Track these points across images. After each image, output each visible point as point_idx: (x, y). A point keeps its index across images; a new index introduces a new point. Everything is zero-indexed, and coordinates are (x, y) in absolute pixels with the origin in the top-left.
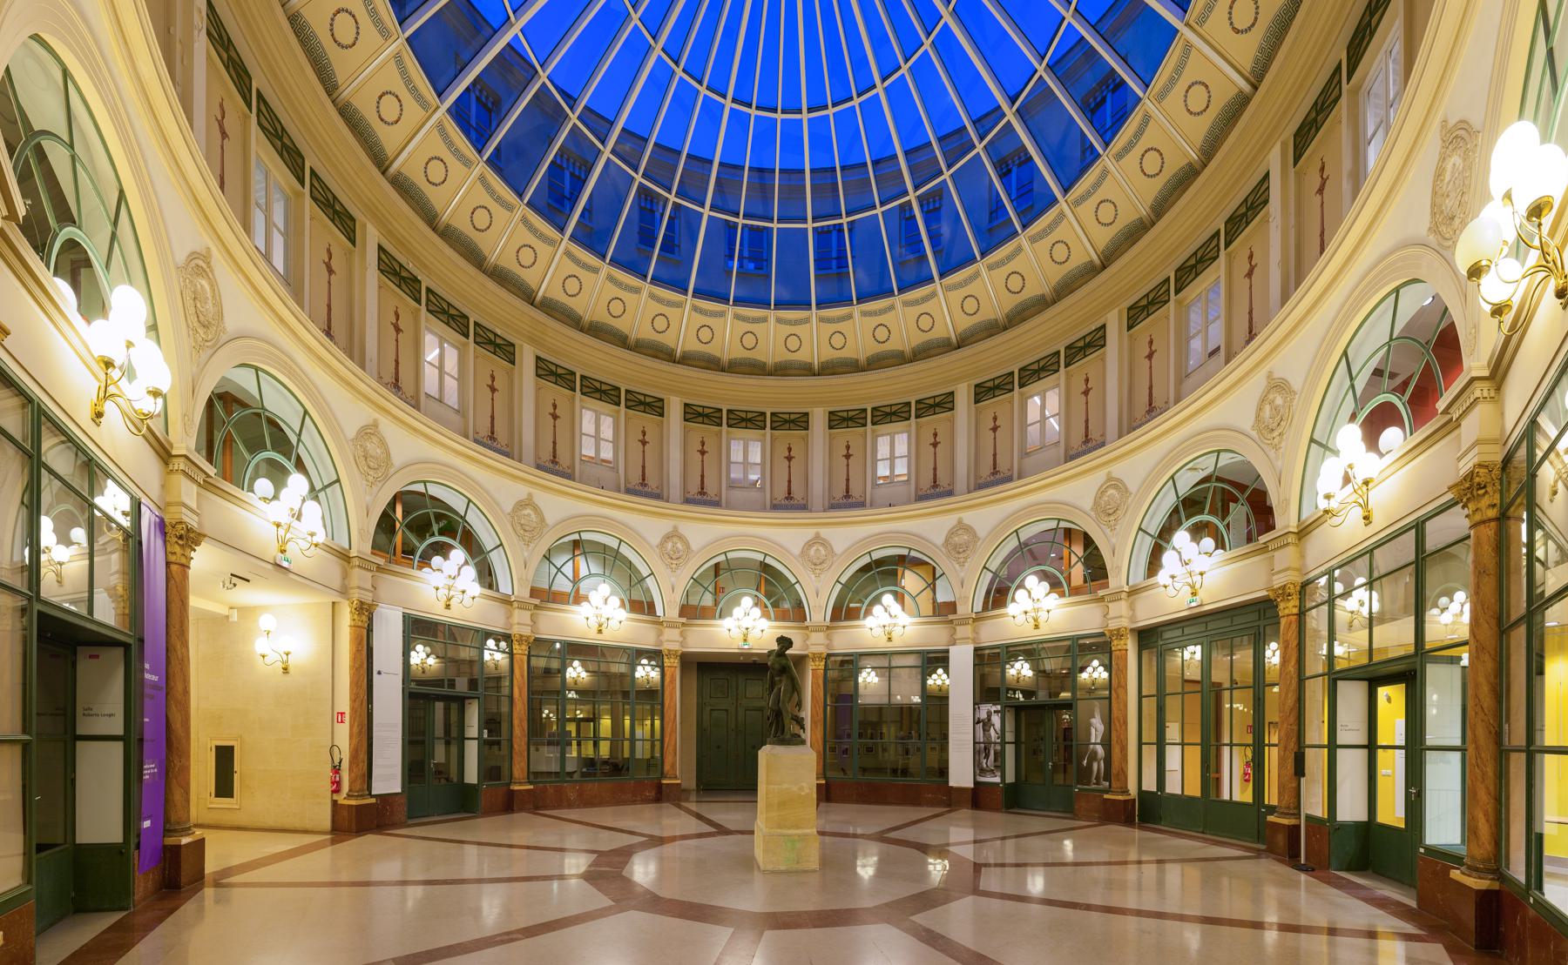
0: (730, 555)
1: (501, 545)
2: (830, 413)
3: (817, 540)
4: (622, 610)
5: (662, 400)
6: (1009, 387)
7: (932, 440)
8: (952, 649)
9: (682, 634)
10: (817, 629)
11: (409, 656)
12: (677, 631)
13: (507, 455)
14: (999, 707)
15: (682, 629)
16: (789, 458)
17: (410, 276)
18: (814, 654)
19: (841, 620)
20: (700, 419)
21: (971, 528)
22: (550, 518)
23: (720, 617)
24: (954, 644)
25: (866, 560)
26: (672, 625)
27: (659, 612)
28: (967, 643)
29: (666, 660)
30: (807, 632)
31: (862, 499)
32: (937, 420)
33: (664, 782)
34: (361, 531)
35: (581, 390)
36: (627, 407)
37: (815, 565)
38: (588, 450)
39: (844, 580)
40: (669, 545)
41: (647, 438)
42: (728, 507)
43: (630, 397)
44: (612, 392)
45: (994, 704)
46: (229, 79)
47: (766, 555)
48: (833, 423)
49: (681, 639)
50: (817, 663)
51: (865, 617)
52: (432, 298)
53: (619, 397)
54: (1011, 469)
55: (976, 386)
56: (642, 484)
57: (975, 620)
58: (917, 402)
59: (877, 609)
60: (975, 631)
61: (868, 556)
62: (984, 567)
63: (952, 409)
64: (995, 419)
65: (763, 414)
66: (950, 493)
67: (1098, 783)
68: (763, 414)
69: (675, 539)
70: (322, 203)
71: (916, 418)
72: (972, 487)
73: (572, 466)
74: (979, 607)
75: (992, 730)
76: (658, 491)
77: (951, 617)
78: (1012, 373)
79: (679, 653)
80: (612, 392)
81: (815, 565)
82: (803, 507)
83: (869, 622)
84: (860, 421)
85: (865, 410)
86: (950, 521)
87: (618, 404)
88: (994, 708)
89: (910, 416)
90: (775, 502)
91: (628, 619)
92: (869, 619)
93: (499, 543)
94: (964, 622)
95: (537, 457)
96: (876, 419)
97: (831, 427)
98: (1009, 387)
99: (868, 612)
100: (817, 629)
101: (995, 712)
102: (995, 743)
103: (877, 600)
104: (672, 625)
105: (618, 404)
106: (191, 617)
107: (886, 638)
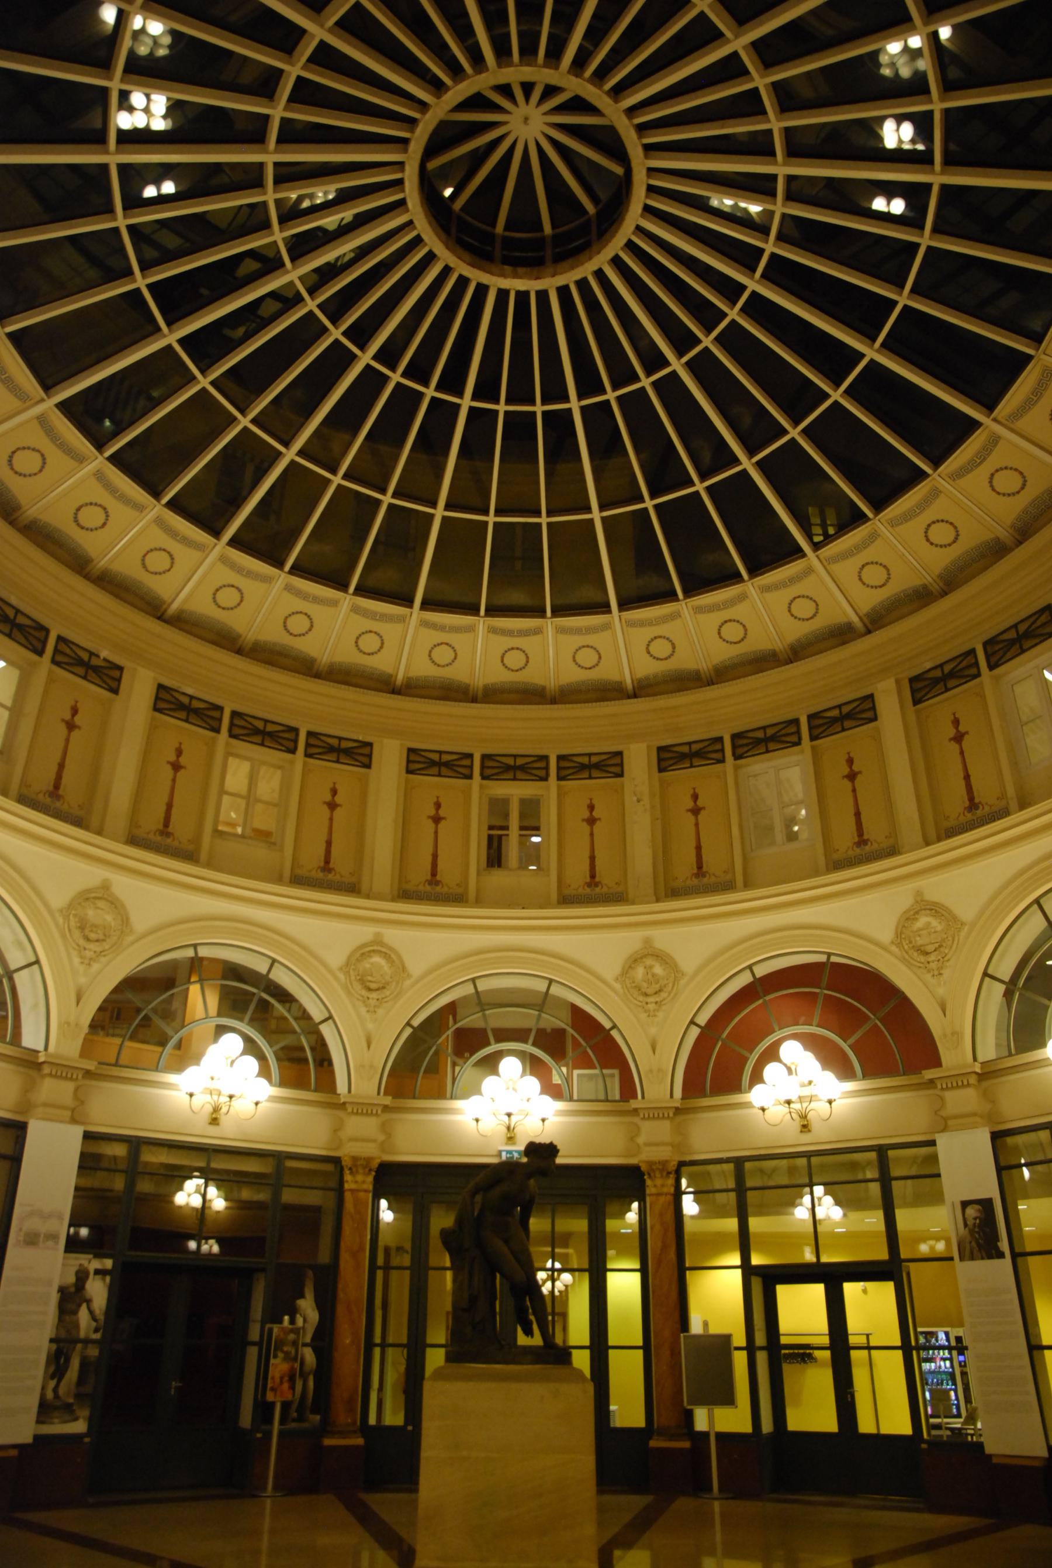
0: (482, 986)
1: (37, 962)
2: (660, 749)
3: (648, 953)
4: (263, 1082)
5: (370, 745)
6: (973, 671)
7: (846, 770)
8: (943, 1142)
9: (384, 1127)
10: (656, 1114)
11: (675, 1191)
12: (70, 1086)
13: (78, 822)
14: (109, 1263)
15: (387, 1116)
16: (591, 821)
17: (33, 624)
18: (355, 1159)
19: (703, 1095)
20: (435, 770)
21: (123, 906)
22: (140, 922)
23: (451, 1098)
24: (945, 1129)
25: (745, 979)
26: (363, 1109)
27: (341, 1087)
28: (973, 1126)
29: (348, 1177)
30: (636, 1120)
31: (729, 877)
32: (855, 739)
33: (328, 1442)
34: (64, 1024)
35: (230, 730)
36: (307, 755)
37: (646, 995)
38: (231, 813)
39: (703, 1019)
40: (640, 972)
41: (338, 799)
42: (479, 902)
43: (63, 647)
44: (286, 735)
45: (98, 1256)
46: (842, 1155)
47: (551, 981)
48: (664, 764)
49: (381, 1138)
50: (659, 1182)
51: (751, 1087)
52: (39, 646)
53: (296, 741)
54: (1003, 796)
55: (912, 680)
56: (430, 883)
57: (982, 1077)
58: (811, 717)
59: (771, 1071)
60: (79, 1099)
61: (748, 972)
62: (986, 974)
63: (875, 719)
64: (956, 722)
65: (545, 758)
66: (892, 851)
67: (301, 1419)
68: (545, 758)
69: (649, 962)
70: (170, 710)
71: (813, 738)
72: (932, 834)
73: (197, 840)
74: (988, 1051)
75: (83, 1314)
76: (191, 847)
77: (929, 1074)
78: (972, 652)
79: (375, 1165)
80: (286, 735)
81: (646, 995)
82: (618, 898)
83: (757, 1096)
84: (714, 756)
85: (720, 740)
86: (902, 897)
87: (293, 751)
88: (95, 1264)
89: (800, 739)
90: (567, 892)
91: (273, 1099)
92: (758, 1088)
93: (33, 959)
94: (958, 1081)
95: (133, 821)
96: (739, 751)
97: (661, 770)
98: (973, 671)
99: (757, 1078)
100: (656, 1114)
101: (97, 1272)
102: (87, 1342)
103: (772, 1054)
104: (363, 1109)
105: (40, 653)
106: (686, 1237)
107: (797, 1123)
